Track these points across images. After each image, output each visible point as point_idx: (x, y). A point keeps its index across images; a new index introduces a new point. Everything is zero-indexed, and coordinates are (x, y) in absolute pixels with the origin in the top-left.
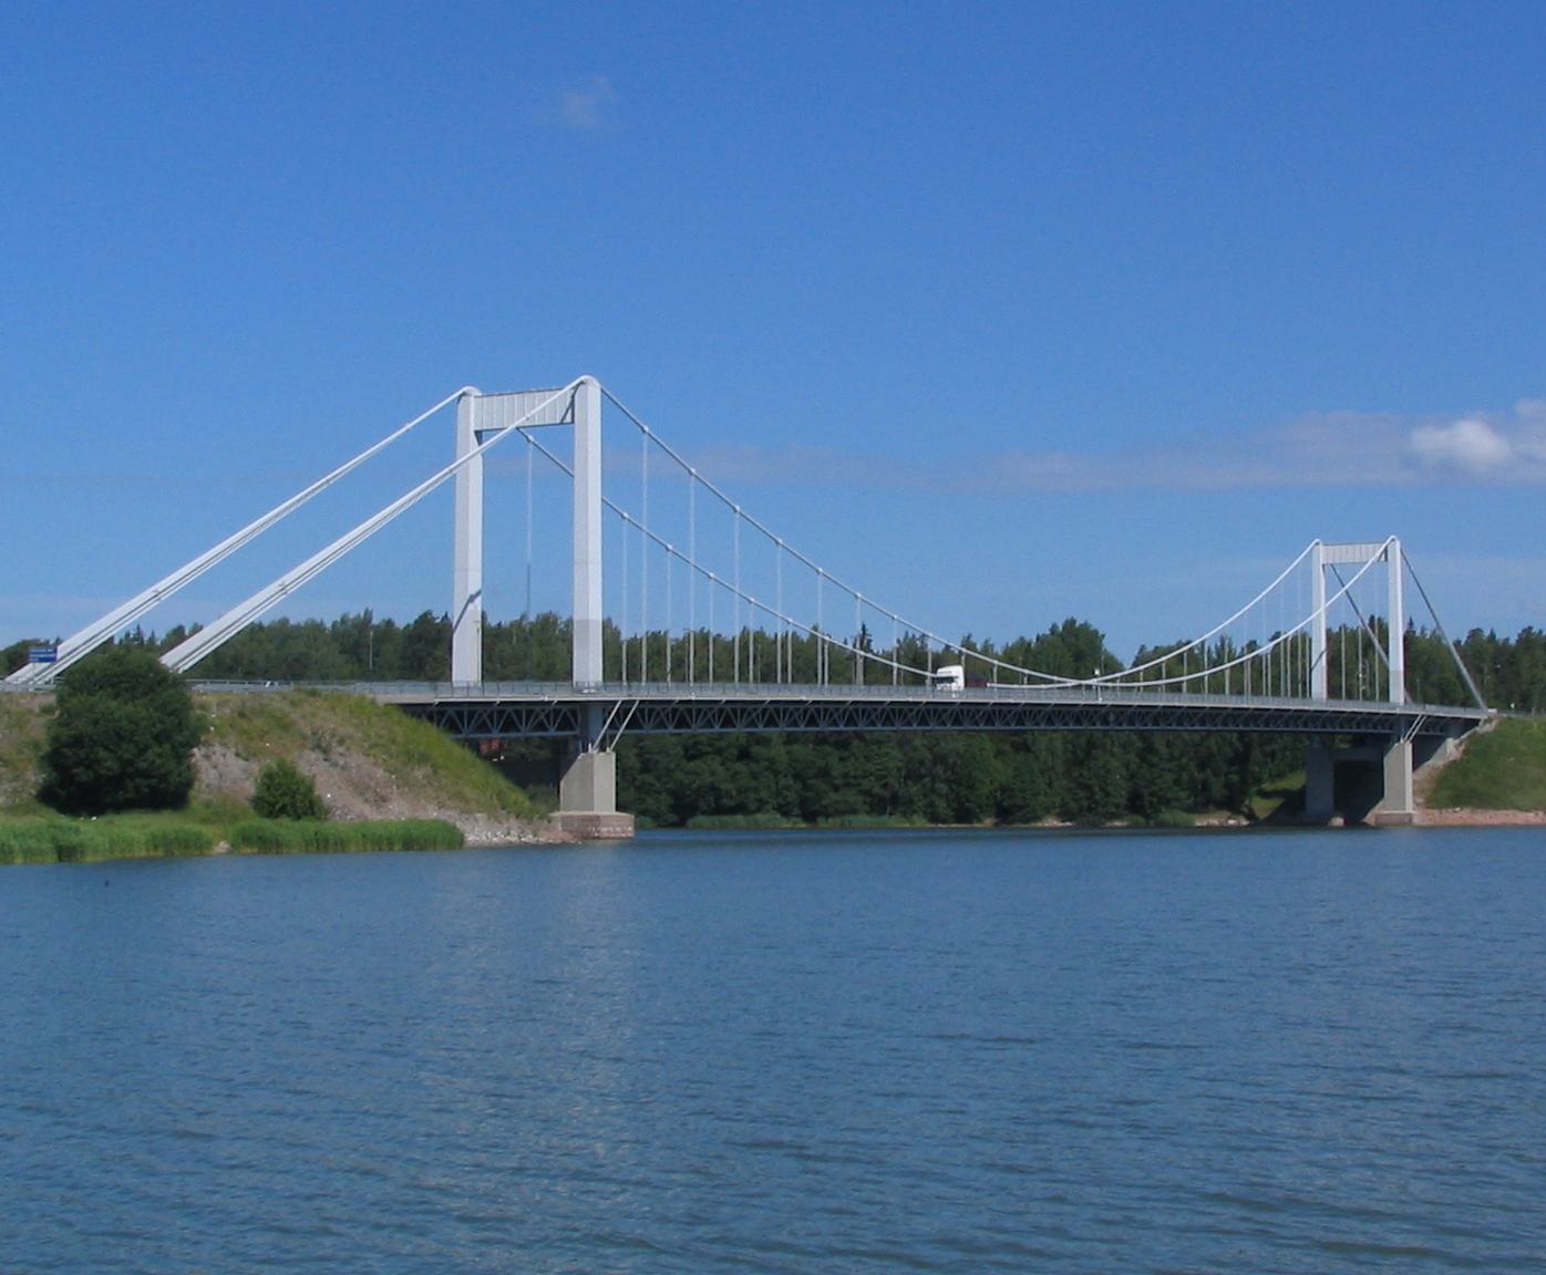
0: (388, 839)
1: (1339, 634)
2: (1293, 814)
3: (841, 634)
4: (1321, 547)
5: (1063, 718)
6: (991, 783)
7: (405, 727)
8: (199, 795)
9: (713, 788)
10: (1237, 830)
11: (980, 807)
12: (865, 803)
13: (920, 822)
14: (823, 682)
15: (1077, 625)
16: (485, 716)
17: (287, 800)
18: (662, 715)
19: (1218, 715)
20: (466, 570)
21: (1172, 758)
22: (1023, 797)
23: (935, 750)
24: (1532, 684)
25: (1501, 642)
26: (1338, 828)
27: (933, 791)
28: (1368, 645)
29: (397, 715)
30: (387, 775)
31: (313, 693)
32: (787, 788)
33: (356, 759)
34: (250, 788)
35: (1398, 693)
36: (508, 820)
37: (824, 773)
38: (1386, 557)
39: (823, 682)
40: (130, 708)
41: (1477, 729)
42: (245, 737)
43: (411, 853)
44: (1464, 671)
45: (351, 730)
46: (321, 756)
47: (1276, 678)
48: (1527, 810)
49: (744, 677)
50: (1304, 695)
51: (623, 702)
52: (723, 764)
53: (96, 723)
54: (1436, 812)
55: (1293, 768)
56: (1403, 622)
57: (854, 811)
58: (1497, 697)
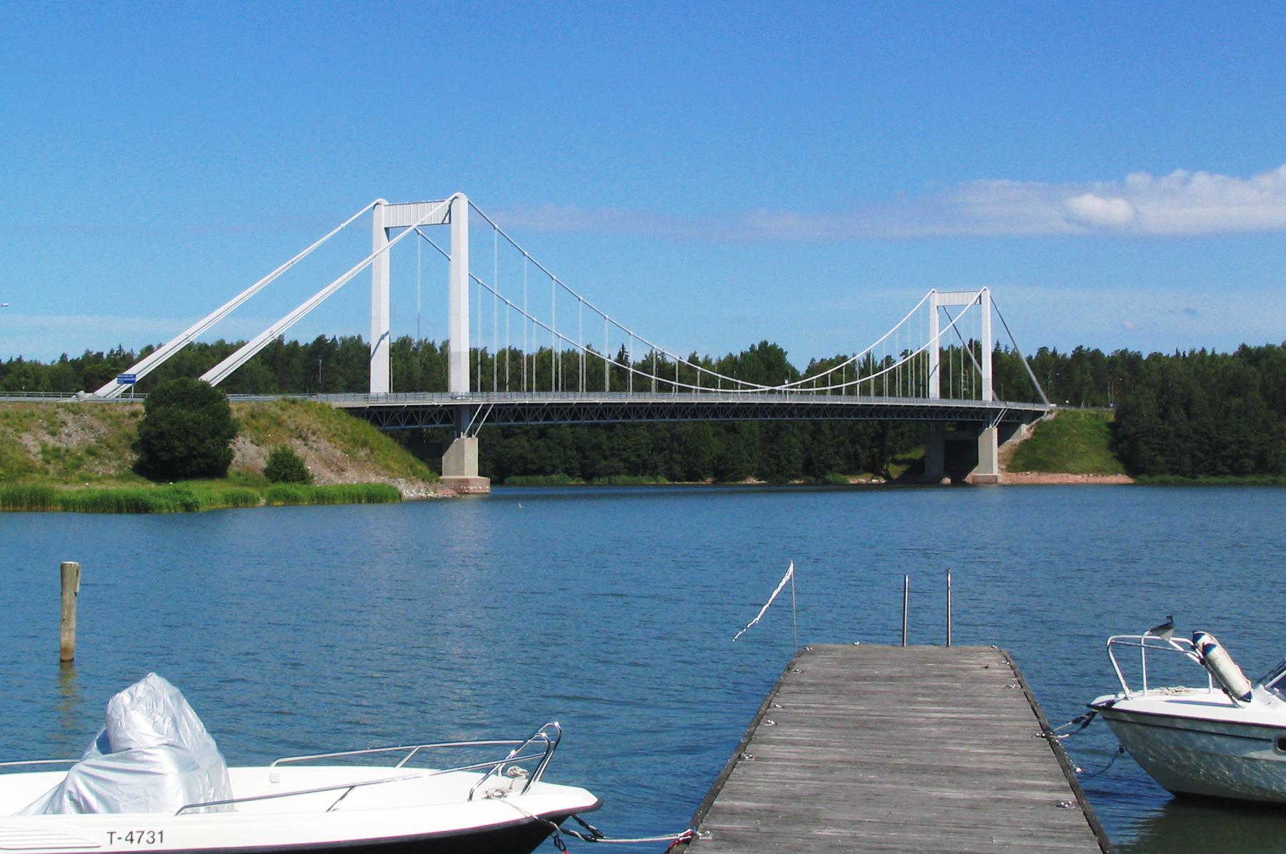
0: (358, 495)
1: (948, 351)
2: (916, 477)
3: (676, 355)
4: (936, 294)
5: (725, 412)
6: (711, 454)
7: (351, 423)
8: (233, 469)
9: (521, 457)
10: (877, 487)
11: (703, 470)
12: (625, 468)
13: (663, 480)
14: (583, 391)
15: (769, 345)
16: (397, 415)
17: (288, 470)
18: (507, 413)
19: (866, 410)
20: (380, 319)
21: (834, 438)
22: (733, 464)
23: (673, 431)
24: (1082, 385)
25: (1060, 357)
26: (947, 486)
27: (671, 459)
28: (968, 360)
29: (344, 416)
30: (344, 454)
31: (294, 402)
32: (571, 457)
33: (324, 444)
34: (263, 464)
35: (988, 394)
36: (417, 482)
37: (597, 447)
38: (980, 303)
39: (675, 391)
40: (193, 414)
41: (1042, 417)
42: (256, 430)
44: (1034, 379)
45: (319, 426)
46: (303, 443)
47: (905, 382)
48: (1076, 474)
49: (529, 390)
50: (924, 397)
51: (484, 405)
52: (528, 441)
53: (173, 423)
54: (1014, 474)
55: (916, 445)
56: (992, 341)
57: (617, 473)
58: (1057, 395)
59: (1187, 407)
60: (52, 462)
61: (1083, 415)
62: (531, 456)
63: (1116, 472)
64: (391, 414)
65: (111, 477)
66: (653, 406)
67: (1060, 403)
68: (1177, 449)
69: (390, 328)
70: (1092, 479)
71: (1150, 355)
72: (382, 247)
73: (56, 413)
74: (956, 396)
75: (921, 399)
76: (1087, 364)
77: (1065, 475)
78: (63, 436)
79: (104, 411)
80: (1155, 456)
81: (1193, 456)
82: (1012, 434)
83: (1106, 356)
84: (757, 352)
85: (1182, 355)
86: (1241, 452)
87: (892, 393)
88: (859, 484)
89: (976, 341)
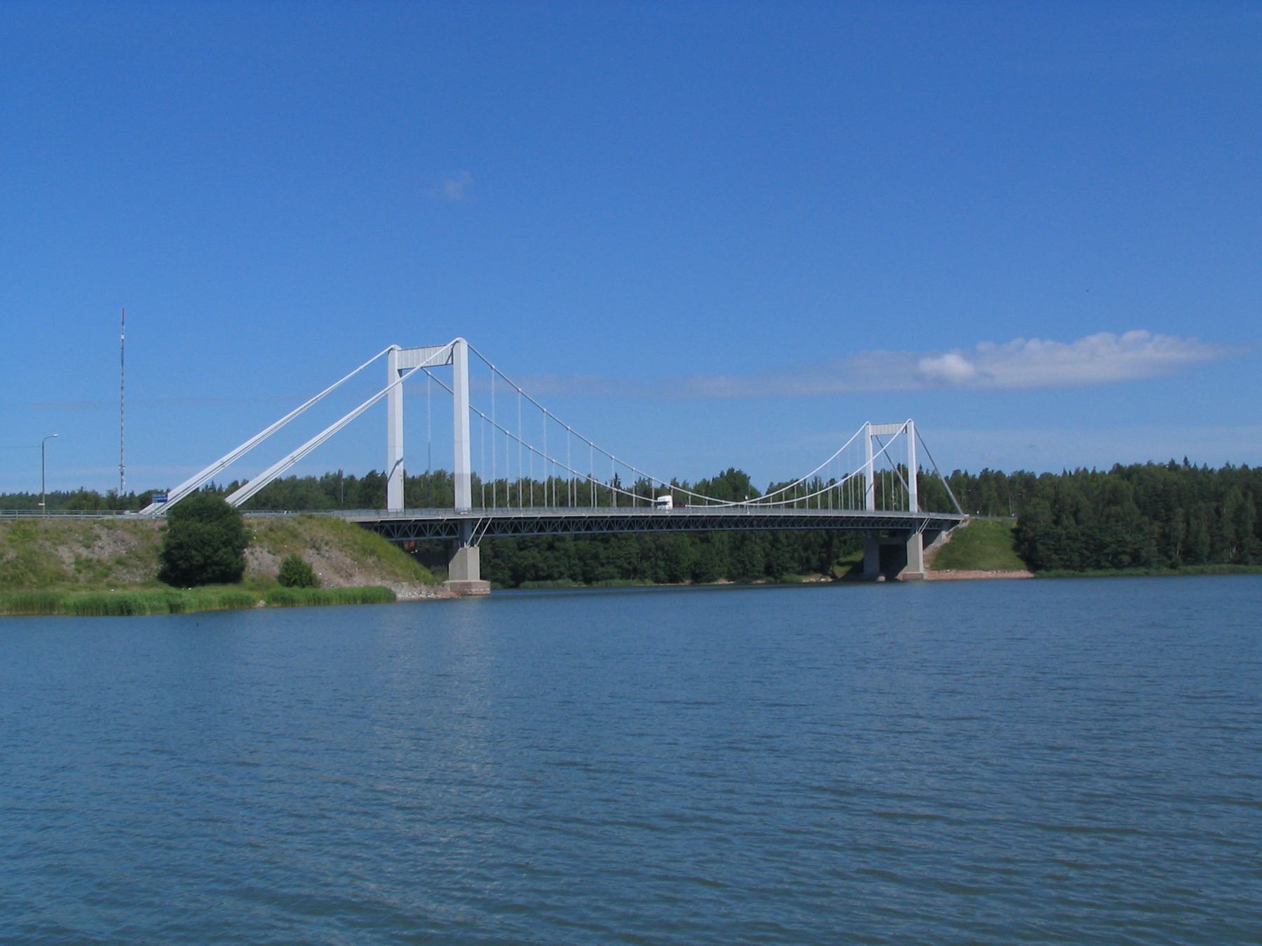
1: (880, 474)
2: (857, 574)
4: (870, 426)
6: (689, 560)
8: (248, 575)
9: (534, 566)
11: (682, 573)
13: (649, 583)
15: (735, 471)
17: (297, 577)
19: (859, 521)
21: (789, 545)
22: (706, 568)
24: (989, 500)
26: (882, 582)
27: (656, 565)
29: (357, 528)
30: (353, 562)
31: (310, 517)
32: (575, 565)
33: (335, 553)
34: (277, 570)
35: (914, 507)
41: (959, 525)
43: (366, 605)
44: (951, 493)
46: (316, 552)
48: (987, 570)
50: (862, 509)
51: (483, 519)
53: (190, 536)
54: (936, 572)
55: (856, 549)
57: (613, 577)
59: (1075, 514)
60: (83, 571)
61: (991, 523)
62: (540, 565)
63: (1019, 569)
64: (402, 528)
65: (136, 584)
66: (633, 519)
67: (971, 515)
68: (1068, 549)
69: (404, 455)
70: (1000, 574)
71: (1042, 475)
72: (396, 390)
73: (91, 528)
74: (887, 508)
75: (859, 511)
76: (993, 483)
78: (97, 549)
79: (135, 526)
80: (1050, 555)
81: (1081, 554)
82: (935, 538)
83: (1007, 476)
84: (726, 477)
85: (1068, 473)
86: (1120, 550)
87: (835, 507)
89: (903, 465)
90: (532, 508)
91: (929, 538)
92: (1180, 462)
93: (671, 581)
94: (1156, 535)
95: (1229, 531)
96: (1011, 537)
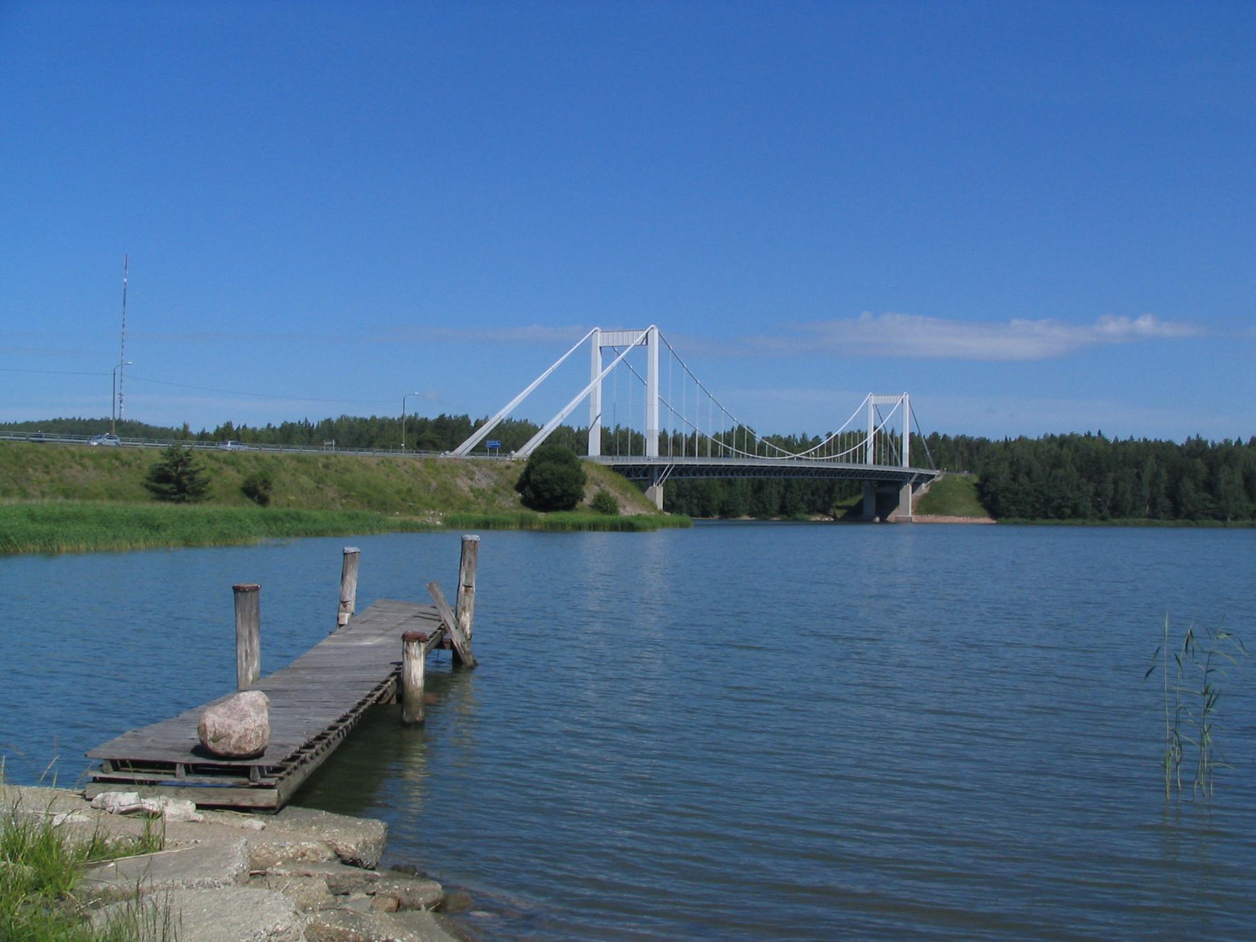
2: (855, 515)
4: (873, 397)
6: (718, 499)
10: (826, 523)
11: (713, 510)
19: (690, 469)
26: (877, 523)
35: (906, 463)
43: (683, 529)
54: (920, 516)
59: (1028, 474)
63: (983, 516)
68: (1023, 502)
77: (952, 517)
88: (817, 521)
90: (683, 458)
91: (916, 486)
92: (1094, 434)
93: (703, 516)
94: (1091, 494)
95: (1146, 492)
96: (974, 490)
